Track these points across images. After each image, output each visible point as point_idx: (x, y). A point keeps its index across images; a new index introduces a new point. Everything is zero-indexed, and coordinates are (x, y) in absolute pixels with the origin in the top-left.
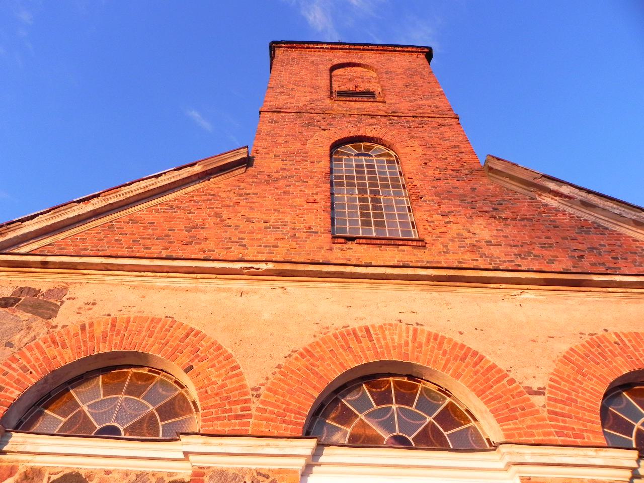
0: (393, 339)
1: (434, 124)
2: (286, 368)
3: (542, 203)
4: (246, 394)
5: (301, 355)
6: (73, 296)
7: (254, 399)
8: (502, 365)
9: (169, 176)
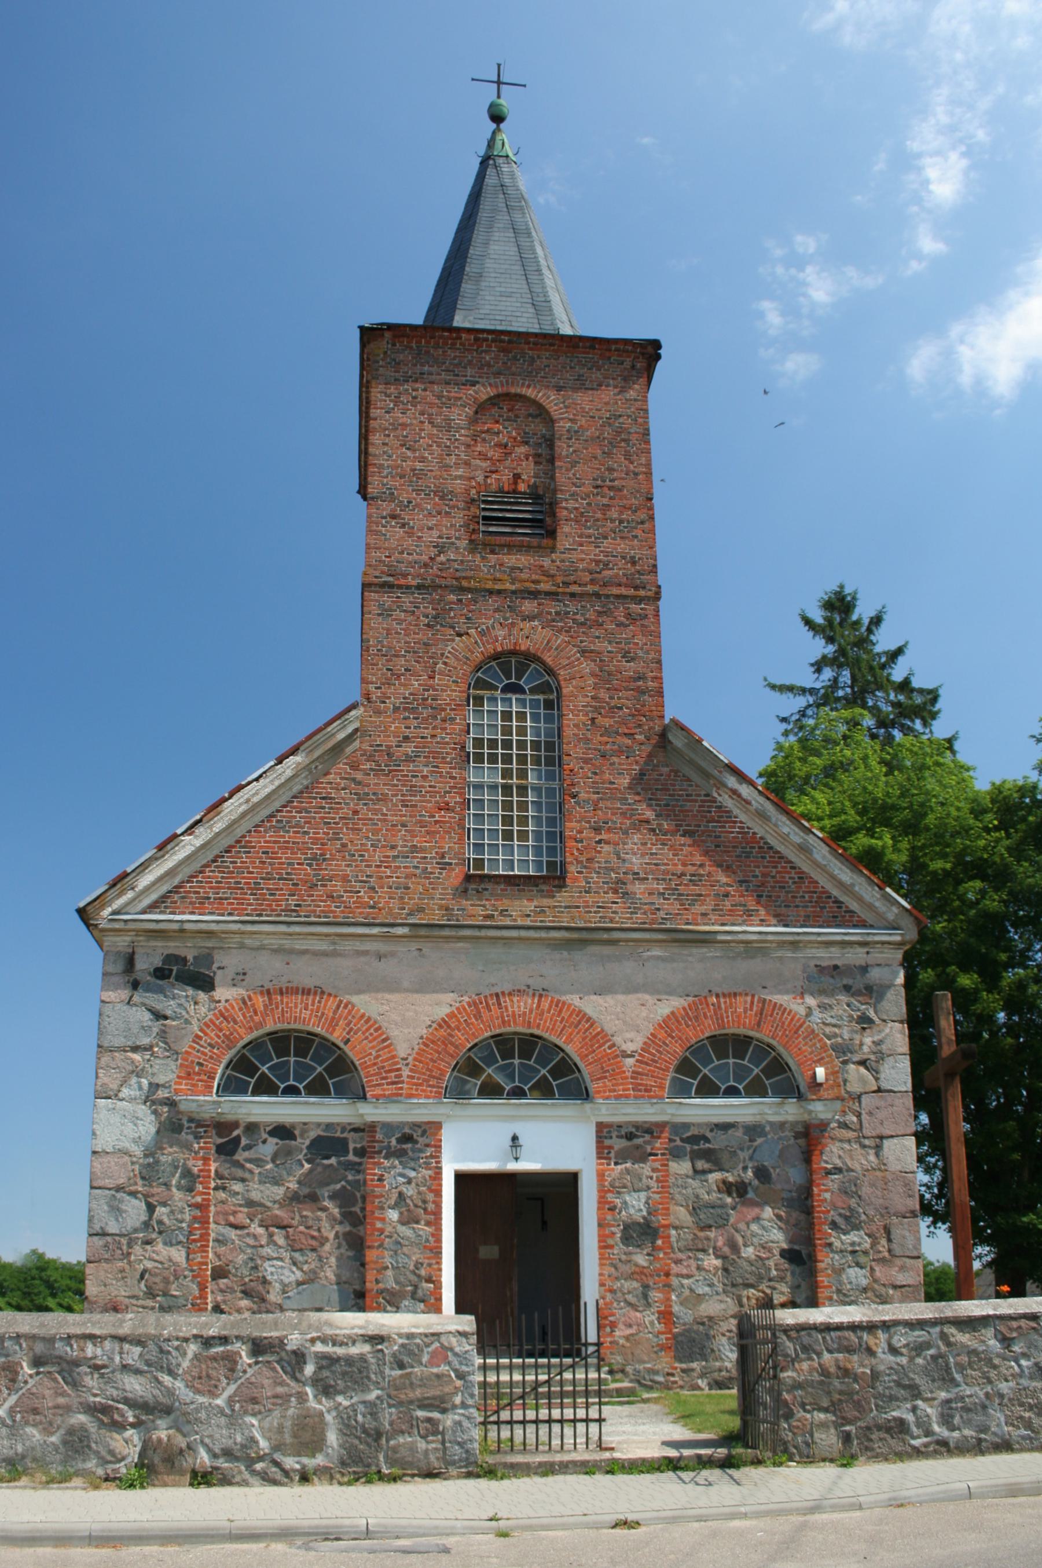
0: (519, 1007)
1: (620, 615)
2: (427, 1038)
3: (715, 802)
4: (397, 1063)
5: (440, 1026)
6: (222, 965)
7: (404, 1068)
8: (609, 1028)
9: (271, 778)
